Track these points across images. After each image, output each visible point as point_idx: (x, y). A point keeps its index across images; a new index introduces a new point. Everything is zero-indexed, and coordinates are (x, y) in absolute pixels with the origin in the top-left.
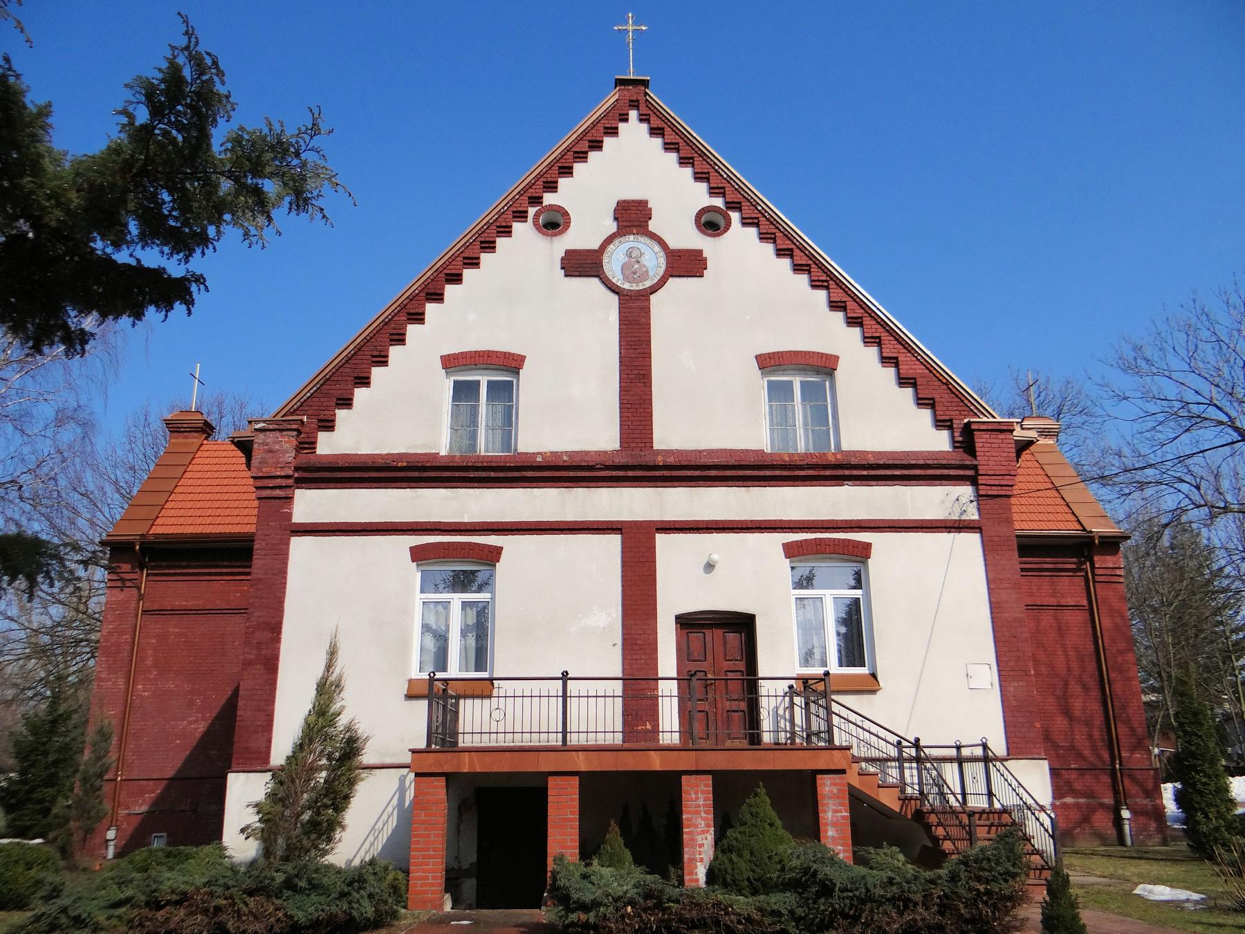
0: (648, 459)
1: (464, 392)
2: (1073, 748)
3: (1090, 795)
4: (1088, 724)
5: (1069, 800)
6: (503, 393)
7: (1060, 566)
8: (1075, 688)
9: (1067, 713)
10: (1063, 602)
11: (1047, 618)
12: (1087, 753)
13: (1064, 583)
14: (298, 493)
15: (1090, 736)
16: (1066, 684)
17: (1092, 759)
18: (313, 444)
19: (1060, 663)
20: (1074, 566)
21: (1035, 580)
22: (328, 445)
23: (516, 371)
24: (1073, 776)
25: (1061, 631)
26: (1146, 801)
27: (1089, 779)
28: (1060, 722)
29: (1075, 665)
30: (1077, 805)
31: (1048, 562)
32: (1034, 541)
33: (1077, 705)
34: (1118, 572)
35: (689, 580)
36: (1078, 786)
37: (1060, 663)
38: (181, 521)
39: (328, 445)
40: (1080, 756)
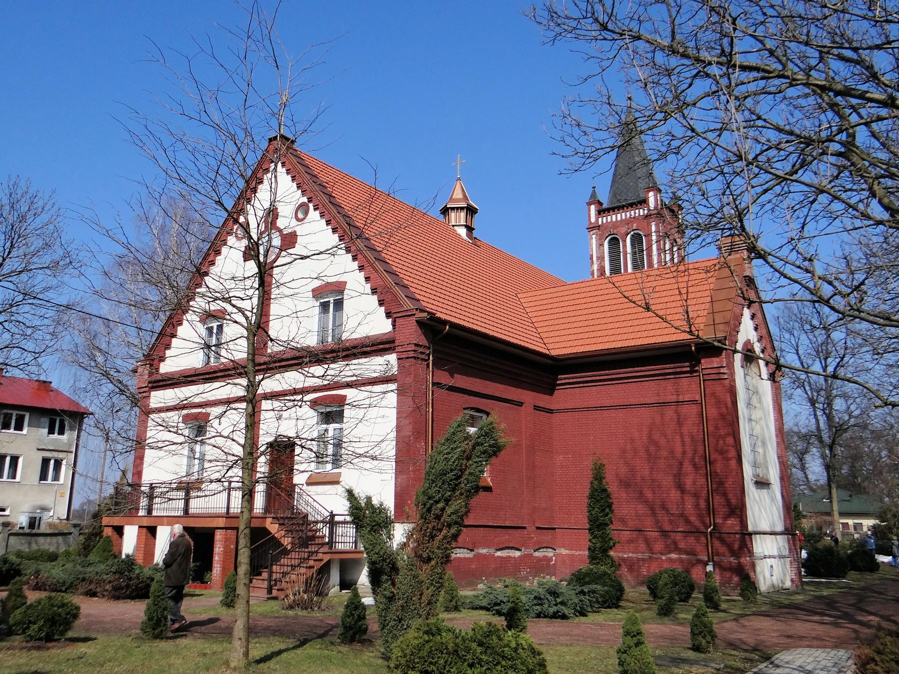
0: (159, 378)
1: (325, 307)
2: (682, 515)
3: (691, 552)
4: (696, 495)
5: (673, 556)
6: (339, 304)
7: (678, 370)
8: (688, 467)
9: (681, 488)
10: (681, 398)
11: (670, 412)
12: (693, 519)
13: (685, 382)
14: (153, 394)
15: (697, 506)
16: (681, 464)
17: (697, 523)
18: (157, 369)
19: (678, 449)
20: (688, 369)
21: (662, 382)
22: (166, 368)
23: (342, 292)
24: (679, 537)
25: (680, 423)
26: (732, 559)
27: (691, 540)
28: (674, 495)
29: (688, 448)
30: (681, 561)
31: (669, 368)
32: (679, 350)
33: (688, 482)
34: (722, 371)
35: (274, 424)
36: (682, 545)
37: (678, 449)
38: (576, 343)
39: (166, 368)
40: (688, 521)
